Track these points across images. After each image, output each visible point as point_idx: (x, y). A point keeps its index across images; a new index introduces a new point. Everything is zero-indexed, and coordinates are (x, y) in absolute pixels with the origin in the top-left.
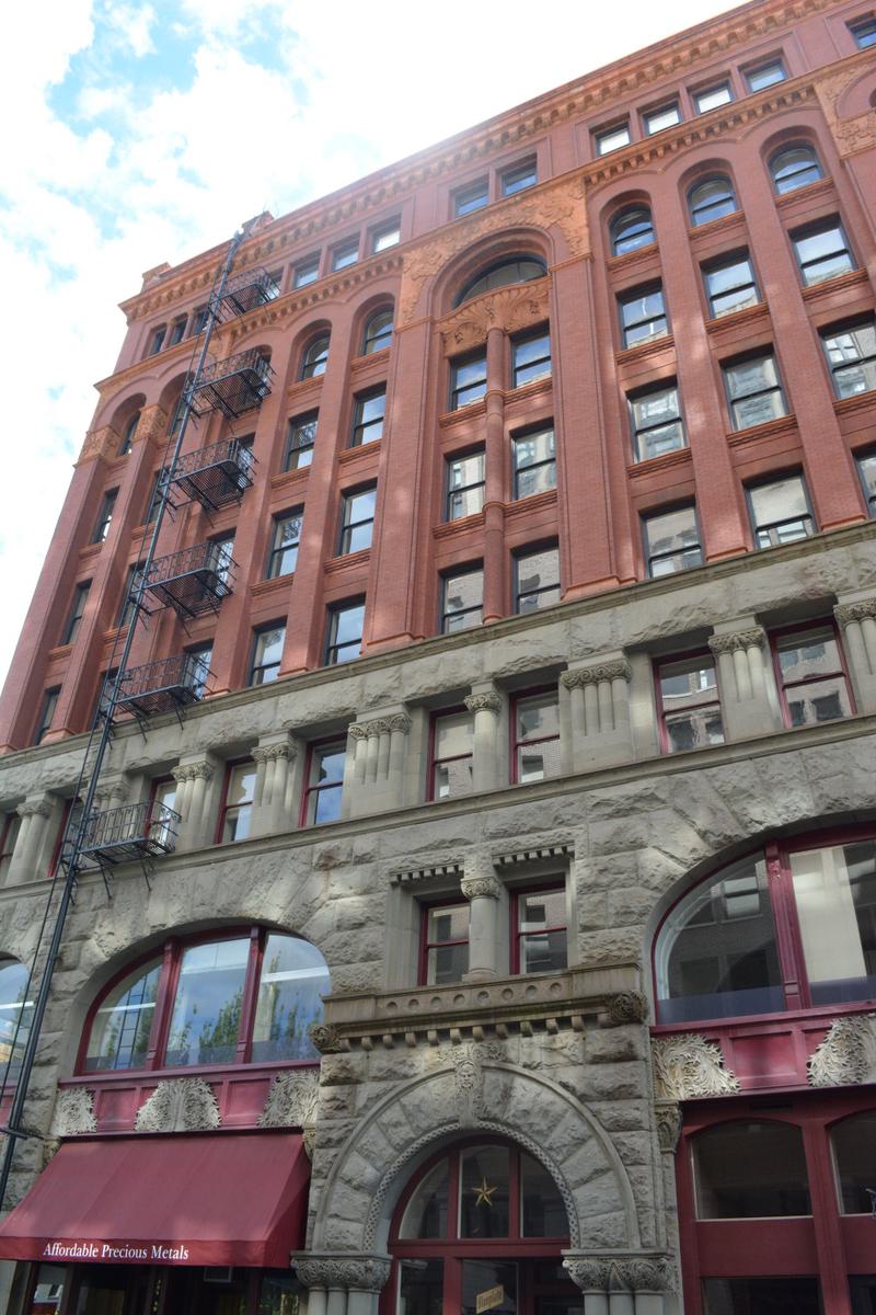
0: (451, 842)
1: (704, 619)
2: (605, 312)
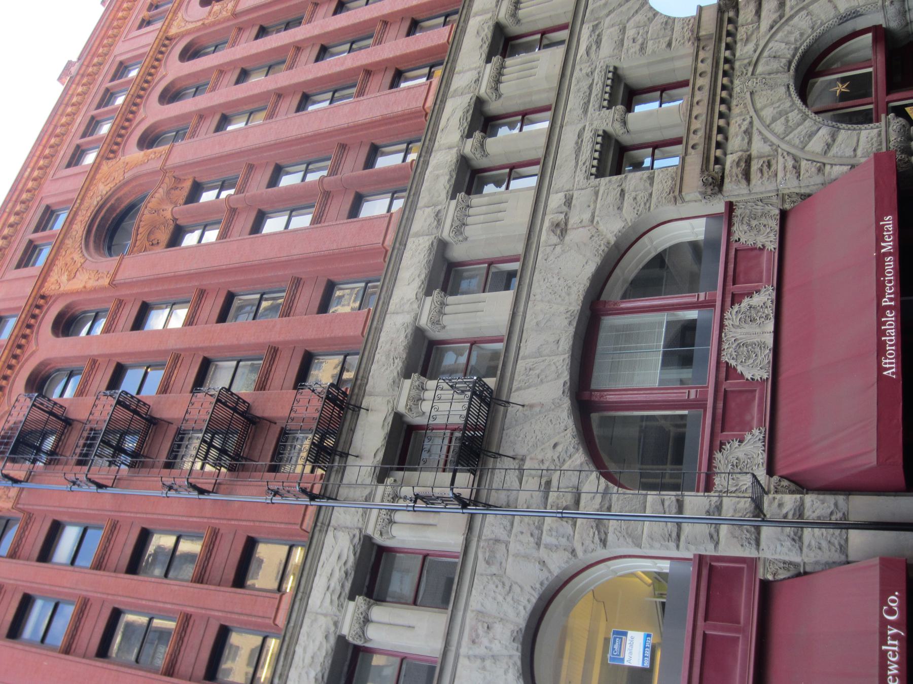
0: (579, 138)
1: (491, 24)
2: (45, 652)
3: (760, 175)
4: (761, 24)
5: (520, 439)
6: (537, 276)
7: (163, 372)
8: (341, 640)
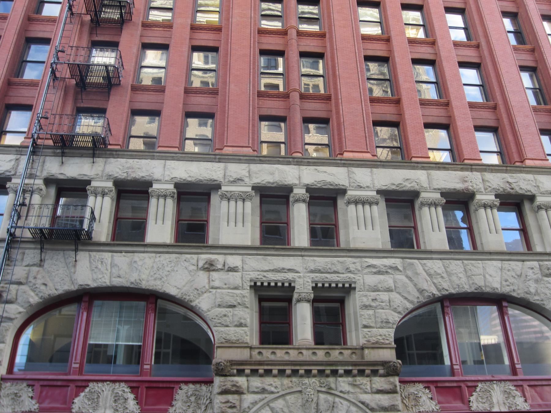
1: (417, 188)
3: (223, 401)
4: (370, 395)
5: (55, 262)
6: (174, 256)
7: (466, 40)
8: (88, 182)
